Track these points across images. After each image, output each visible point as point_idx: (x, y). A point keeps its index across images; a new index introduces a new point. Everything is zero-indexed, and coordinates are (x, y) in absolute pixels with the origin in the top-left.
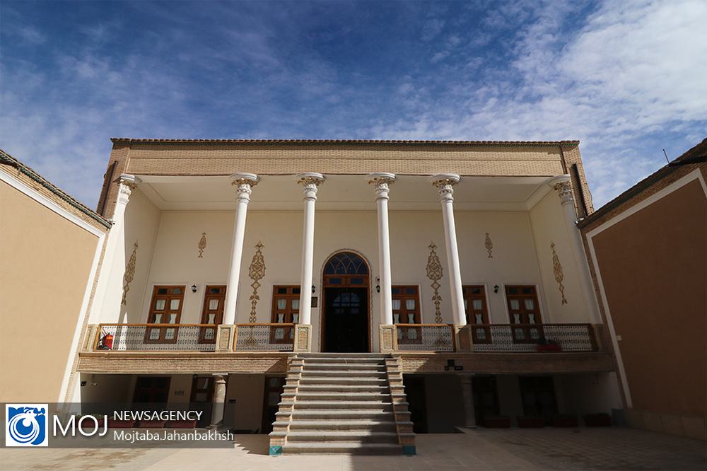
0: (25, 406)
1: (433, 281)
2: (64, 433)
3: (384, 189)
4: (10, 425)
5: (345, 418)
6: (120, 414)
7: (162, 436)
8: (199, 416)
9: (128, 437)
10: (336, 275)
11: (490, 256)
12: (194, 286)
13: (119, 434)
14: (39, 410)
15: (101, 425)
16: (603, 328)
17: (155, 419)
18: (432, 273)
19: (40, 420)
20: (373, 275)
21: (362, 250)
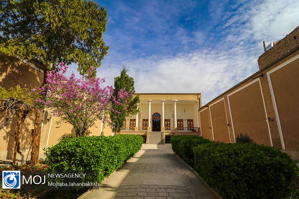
6: (51, 175)
7: (68, 184)
8: (84, 176)
9: (54, 185)
10: (154, 117)
11: (185, 114)
13: (50, 183)
14: (17, 173)
16: (200, 128)
17: (66, 177)
19: (17, 177)
21: (159, 112)
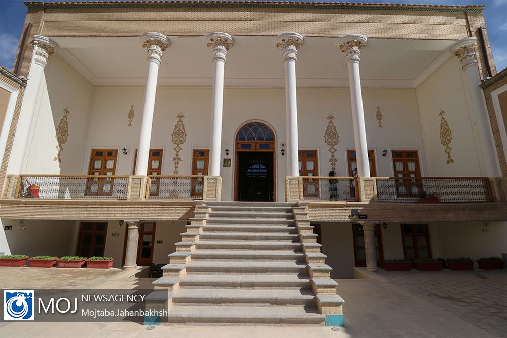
0: (18, 291)
1: (330, 147)
2: (46, 311)
3: (292, 50)
4: (7, 305)
5: (250, 272)
7: (116, 313)
8: (143, 298)
9: (92, 313)
12: (125, 149)
14: (28, 294)
17: (111, 301)
18: (329, 140)
19: (29, 301)
20: (279, 141)
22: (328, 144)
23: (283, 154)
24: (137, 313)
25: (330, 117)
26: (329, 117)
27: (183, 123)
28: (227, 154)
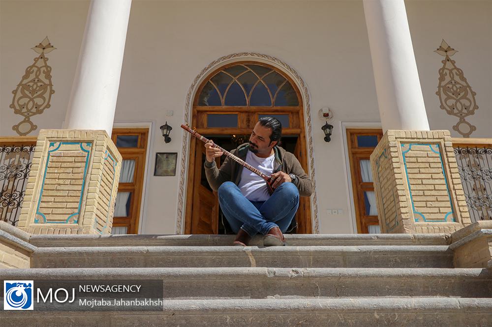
2: (45, 301)
4: (7, 295)
7: (113, 303)
8: (138, 289)
9: (89, 303)
14: (27, 285)
15: (70, 295)
18: (451, 102)
19: (28, 291)
22: (450, 113)
23: (327, 139)
24: (133, 303)
25: (445, 48)
26: (440, 49)
27: (48, 63)
28: (168, 140)
